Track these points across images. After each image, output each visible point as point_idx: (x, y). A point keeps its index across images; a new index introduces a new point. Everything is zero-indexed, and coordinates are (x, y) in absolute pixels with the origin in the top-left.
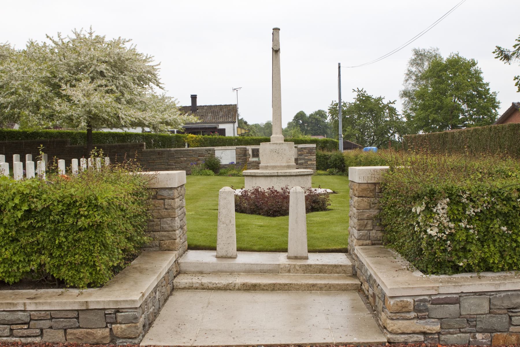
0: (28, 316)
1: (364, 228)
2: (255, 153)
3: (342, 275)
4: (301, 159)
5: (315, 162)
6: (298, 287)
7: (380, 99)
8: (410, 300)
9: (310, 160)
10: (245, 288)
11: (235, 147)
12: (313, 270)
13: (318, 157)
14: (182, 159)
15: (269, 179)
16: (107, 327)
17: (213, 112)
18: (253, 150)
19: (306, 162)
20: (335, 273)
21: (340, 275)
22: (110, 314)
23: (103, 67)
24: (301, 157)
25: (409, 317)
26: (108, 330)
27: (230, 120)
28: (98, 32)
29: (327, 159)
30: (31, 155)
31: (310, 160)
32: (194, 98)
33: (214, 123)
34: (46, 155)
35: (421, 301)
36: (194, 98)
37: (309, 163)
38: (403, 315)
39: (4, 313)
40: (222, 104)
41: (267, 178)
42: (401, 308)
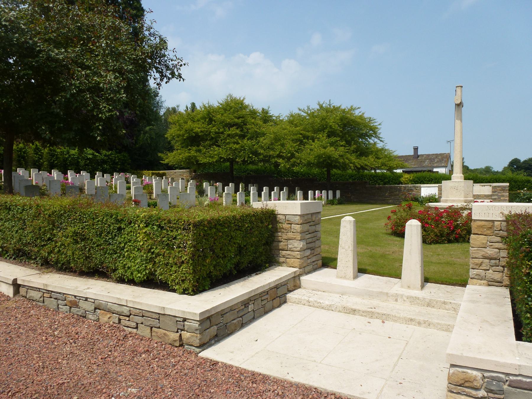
0: (128, 311)
1: (479, 267)
3: (452, 312)
6: (396, 319)
7: (352, 109)
8: (479, 374)
10: (345, 311)
12: (421, 303)
14: (395, 193)
16: (177, 332)
17: (430, 159)
20: (443, 309)
21: (449, 311)
22: (180, 321)
24: (495, 194)
25: (474, 395)
26: (178, 334)
27: (443, 165)
31: (503, 196)
32: (416, 149)
33: (430, 167)
34: (288, 188)
35: (493, 379)
36: (416, 149)
37: (502, 198)
38: (467, 390)
39: (116, 305)
40: (438, 153)
42: (463, 382)
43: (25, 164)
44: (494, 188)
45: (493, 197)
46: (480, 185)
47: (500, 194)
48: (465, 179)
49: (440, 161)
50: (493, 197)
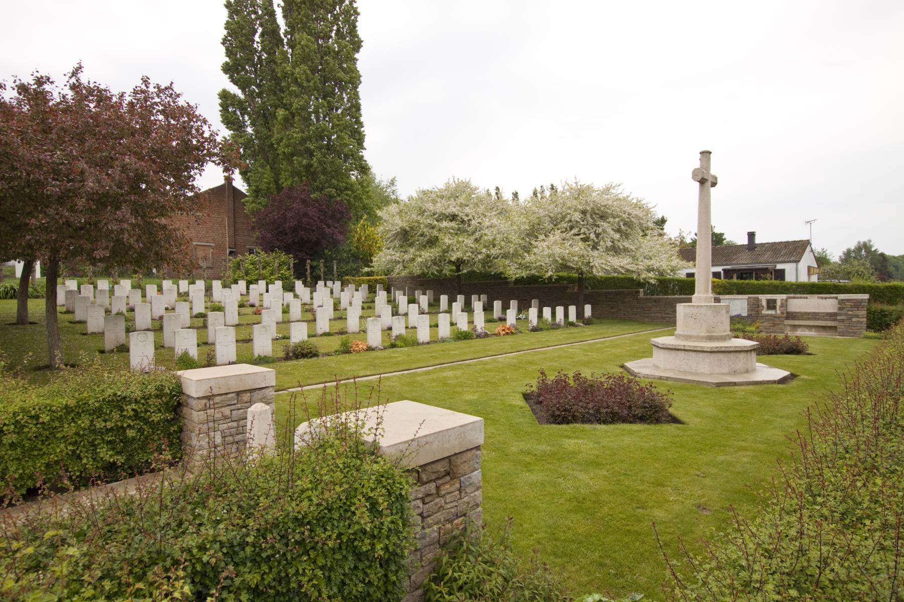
2: (771, 305)
4: (840, 315)
5: (865, 320)
9: (857, 316)
11: (746, 296)
13: (869, 312)
15: (673, 352)
18: (768, 301)
19: (850, 319)
23: (577, 216)
24: (842, 312)
28: (584, 181)
29: (885, 316)
30: (516, 302)
31: (857, 316)
32: (751, 235)
36: (751, 235)
37: (854, 319)
41: (670, 351)
43: (243, 419)
44: (841, 302)
45: (838, 318)
46: (818, 298)
47: (851, 313)
48: (214, 344)
49: (791, 253)
50: (838, 318)
